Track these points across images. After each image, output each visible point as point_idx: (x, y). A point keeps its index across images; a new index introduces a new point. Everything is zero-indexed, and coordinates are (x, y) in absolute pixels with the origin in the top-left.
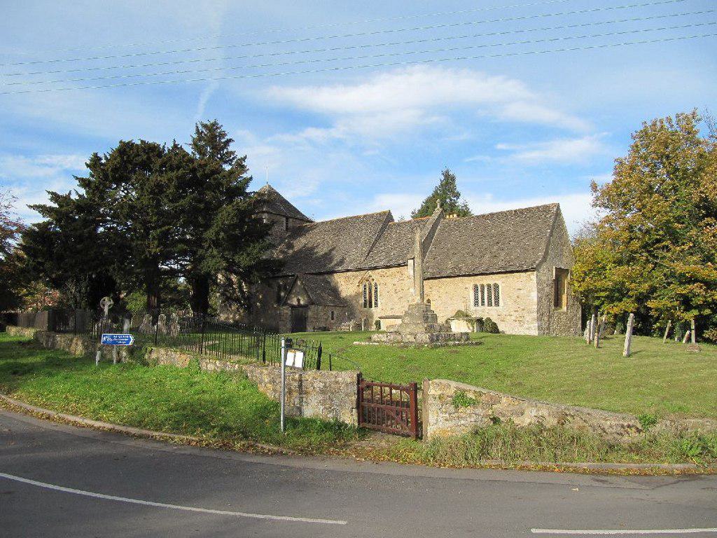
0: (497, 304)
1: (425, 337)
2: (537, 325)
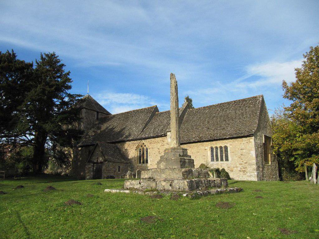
0: (227, 159)
1: (182, 184)
2: (256, 173)
